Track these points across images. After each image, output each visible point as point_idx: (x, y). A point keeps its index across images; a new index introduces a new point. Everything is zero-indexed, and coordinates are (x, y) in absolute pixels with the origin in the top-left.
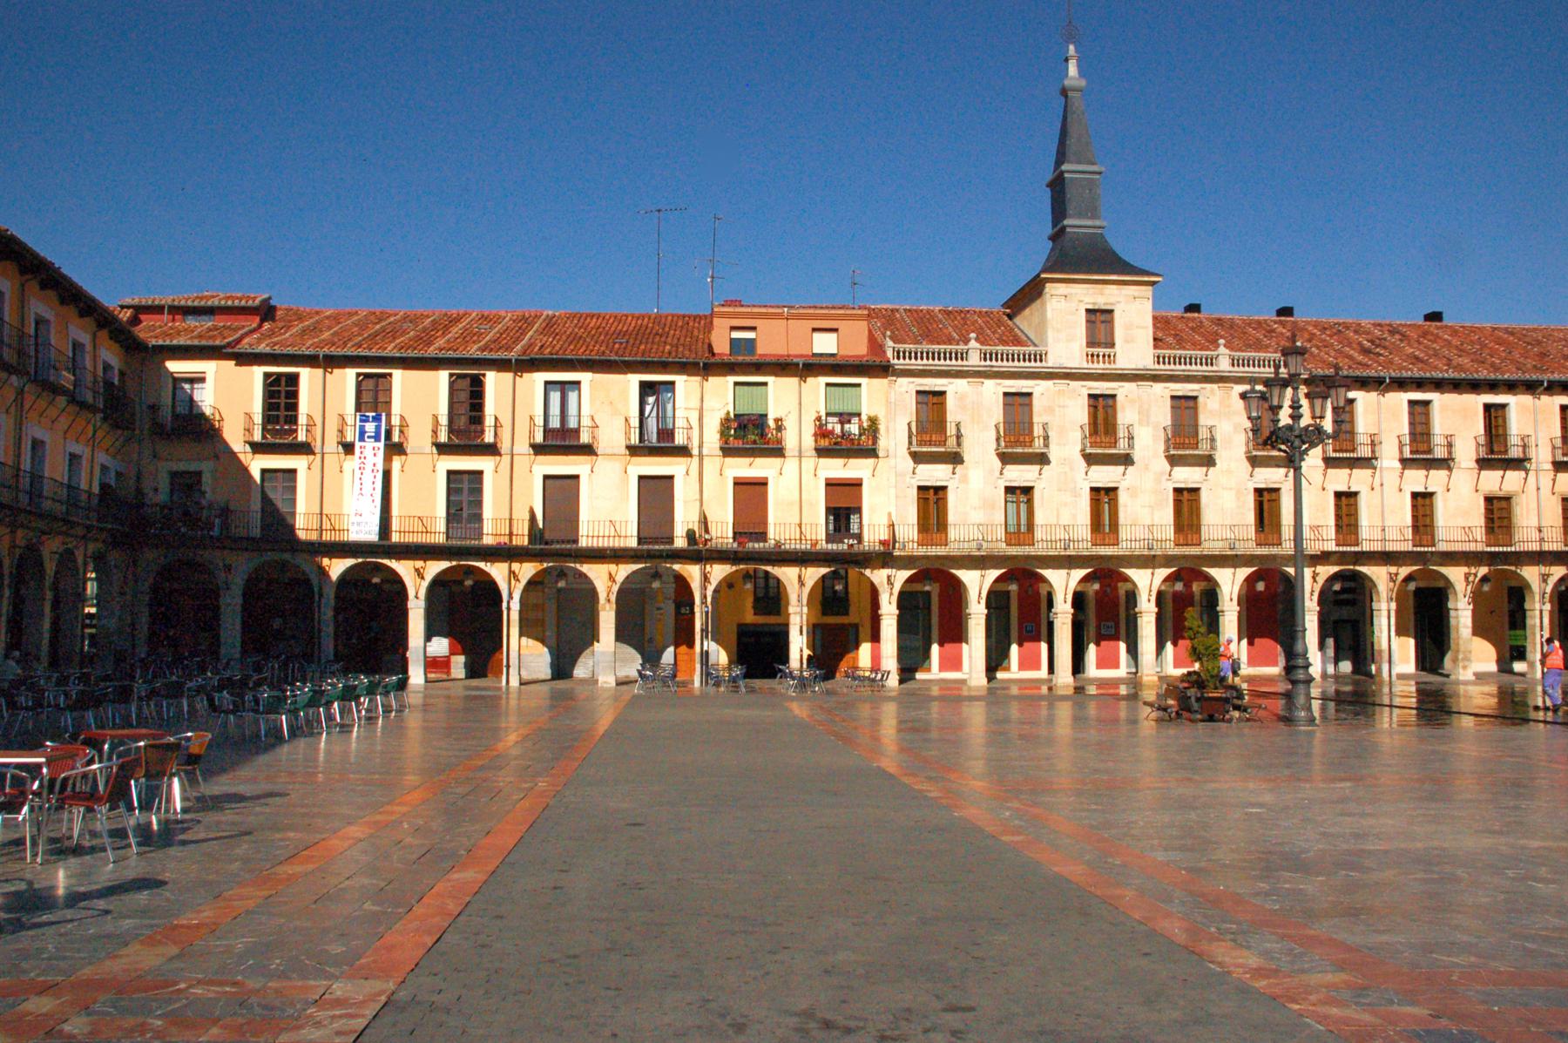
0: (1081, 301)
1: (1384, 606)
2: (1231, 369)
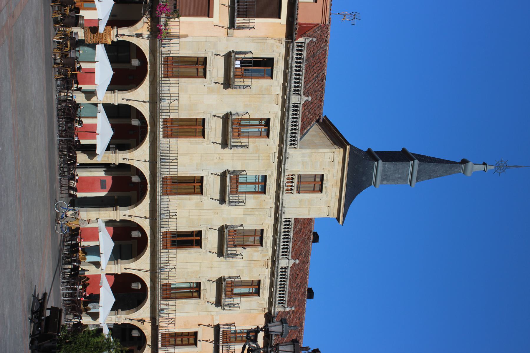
0: (329, 171)
2: (283, 220)
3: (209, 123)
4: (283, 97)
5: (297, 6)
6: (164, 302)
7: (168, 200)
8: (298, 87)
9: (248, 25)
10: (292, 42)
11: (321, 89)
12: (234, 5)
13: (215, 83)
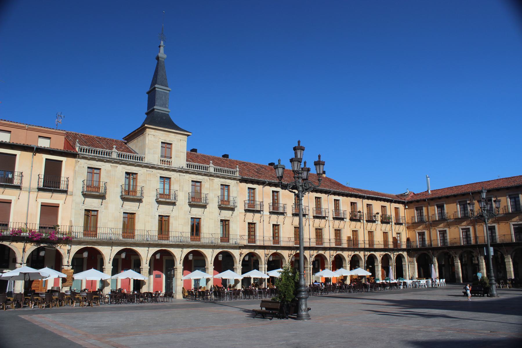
0: (160, 138)
1: (263, 266)
2: (187, 168)
3: (126, 210)
4: (113, 163)
5: (55, 150)
6: (231, 241)
7: (172, 237)
8: (107, 153)
9: (139, 190)
10: (79, 154)
11: (105, 140)
12: (52, 190)
13: (101, 205)
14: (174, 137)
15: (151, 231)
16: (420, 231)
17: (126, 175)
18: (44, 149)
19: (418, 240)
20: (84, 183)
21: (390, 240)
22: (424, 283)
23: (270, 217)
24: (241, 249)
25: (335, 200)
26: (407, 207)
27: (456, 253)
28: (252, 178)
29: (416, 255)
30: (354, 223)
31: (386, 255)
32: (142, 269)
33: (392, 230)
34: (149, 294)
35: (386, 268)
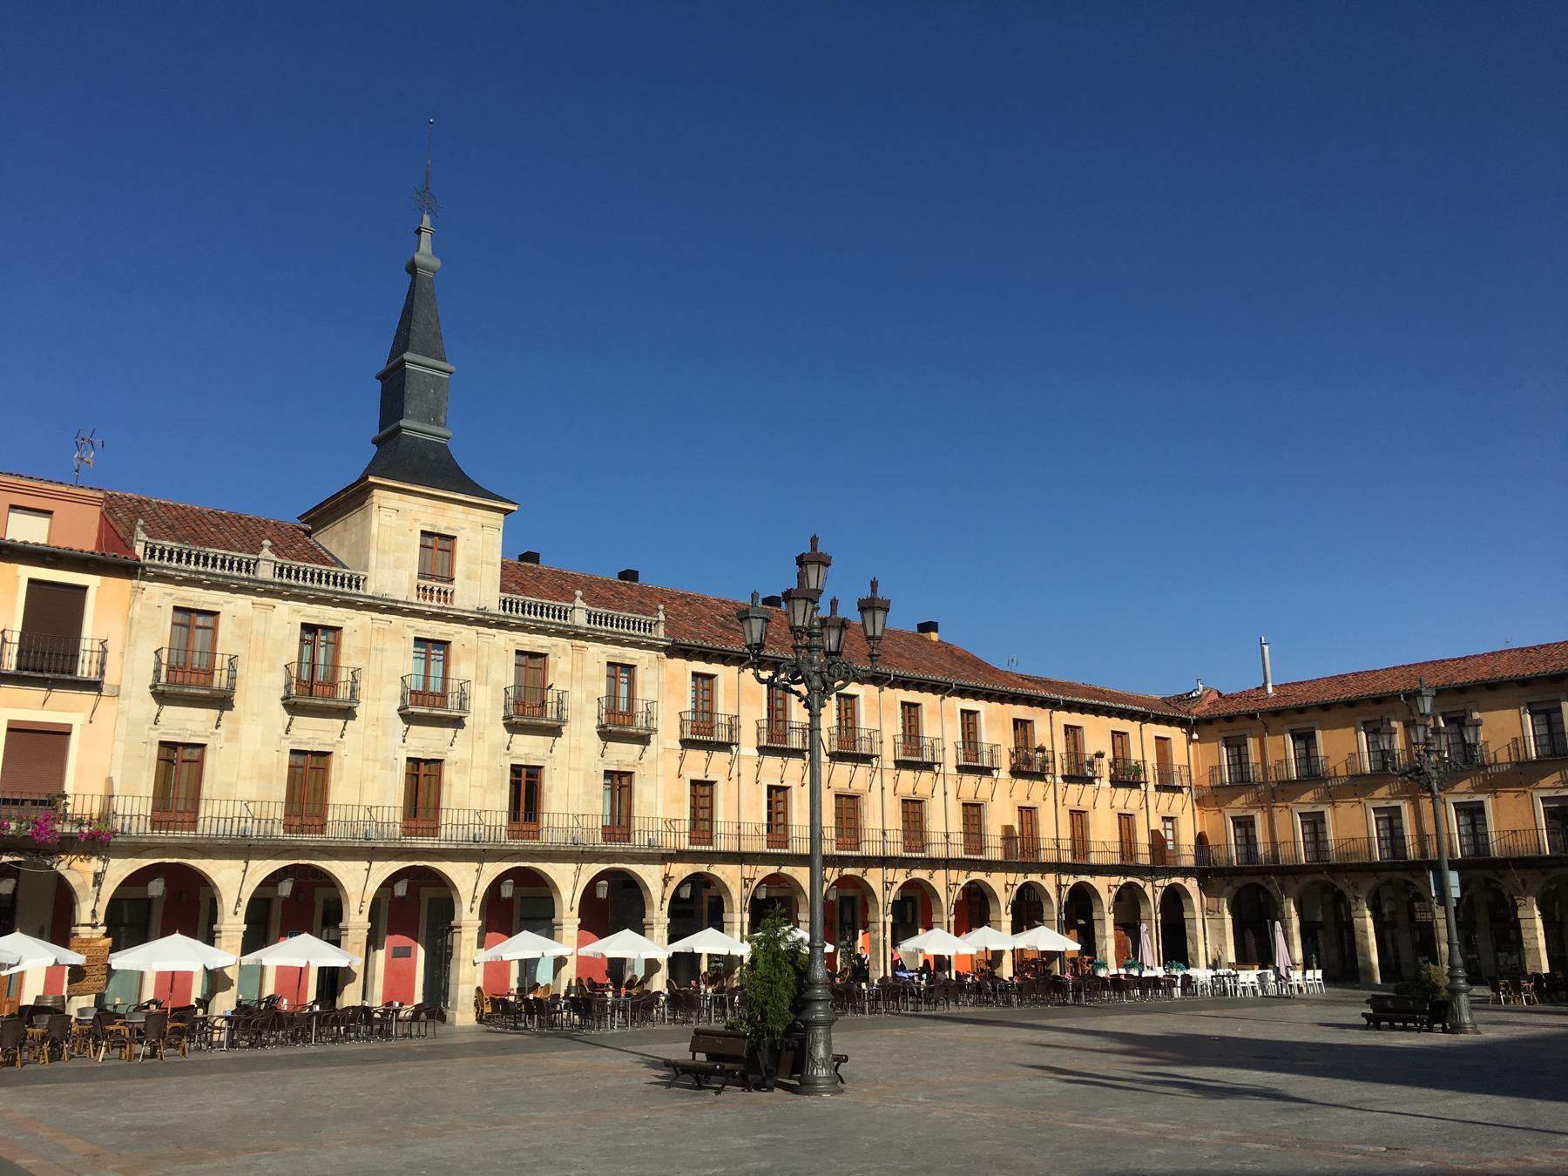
0: (416, 520)
1: (737, 917)
2: (502, 612)
3: (301, 743)
10: (143, 567)
11: (241, 521)
12: (47, 679)
13: (217, 726)
14: (461, 516)
15: (380, 809)
16: (1239, 813)
17: (304, 632)
18: (24, 547)
19: (1233, 842)
20: (158, 657)
21: (1143, 839)
22: (1252, 983)
23: (759, 765)
24: (669, 864)
25: (963, 711)
26: (1195, 736)
27: (1356, 886)
28: (705, 644)
29: (1228, 889)
30: (1022, 784)
31: (1128, 886)
32: (347, 930)
33: (1147, 807)
34: (363, 1014)
35: (1129, 926)
